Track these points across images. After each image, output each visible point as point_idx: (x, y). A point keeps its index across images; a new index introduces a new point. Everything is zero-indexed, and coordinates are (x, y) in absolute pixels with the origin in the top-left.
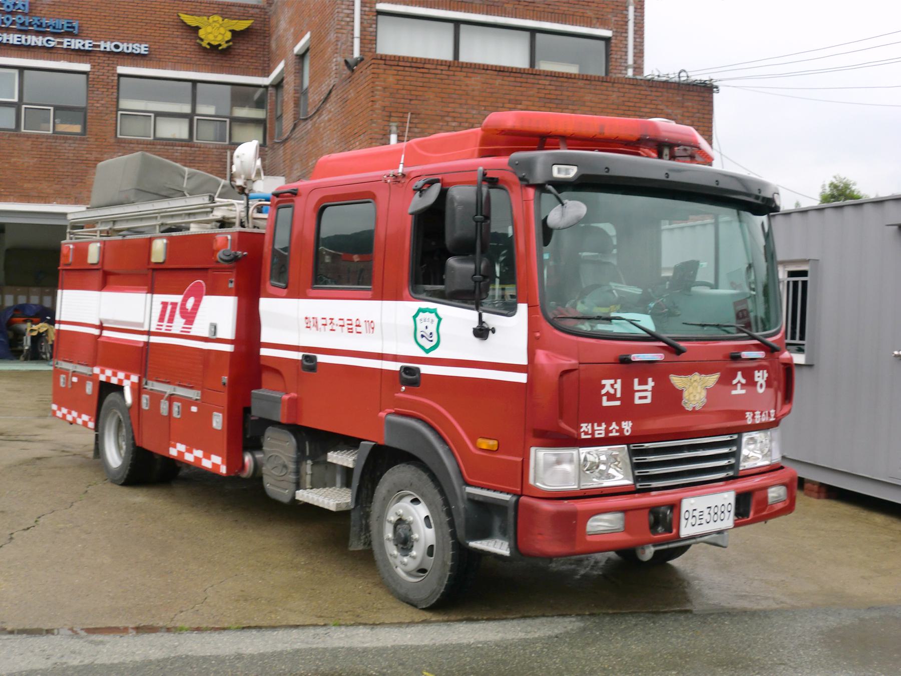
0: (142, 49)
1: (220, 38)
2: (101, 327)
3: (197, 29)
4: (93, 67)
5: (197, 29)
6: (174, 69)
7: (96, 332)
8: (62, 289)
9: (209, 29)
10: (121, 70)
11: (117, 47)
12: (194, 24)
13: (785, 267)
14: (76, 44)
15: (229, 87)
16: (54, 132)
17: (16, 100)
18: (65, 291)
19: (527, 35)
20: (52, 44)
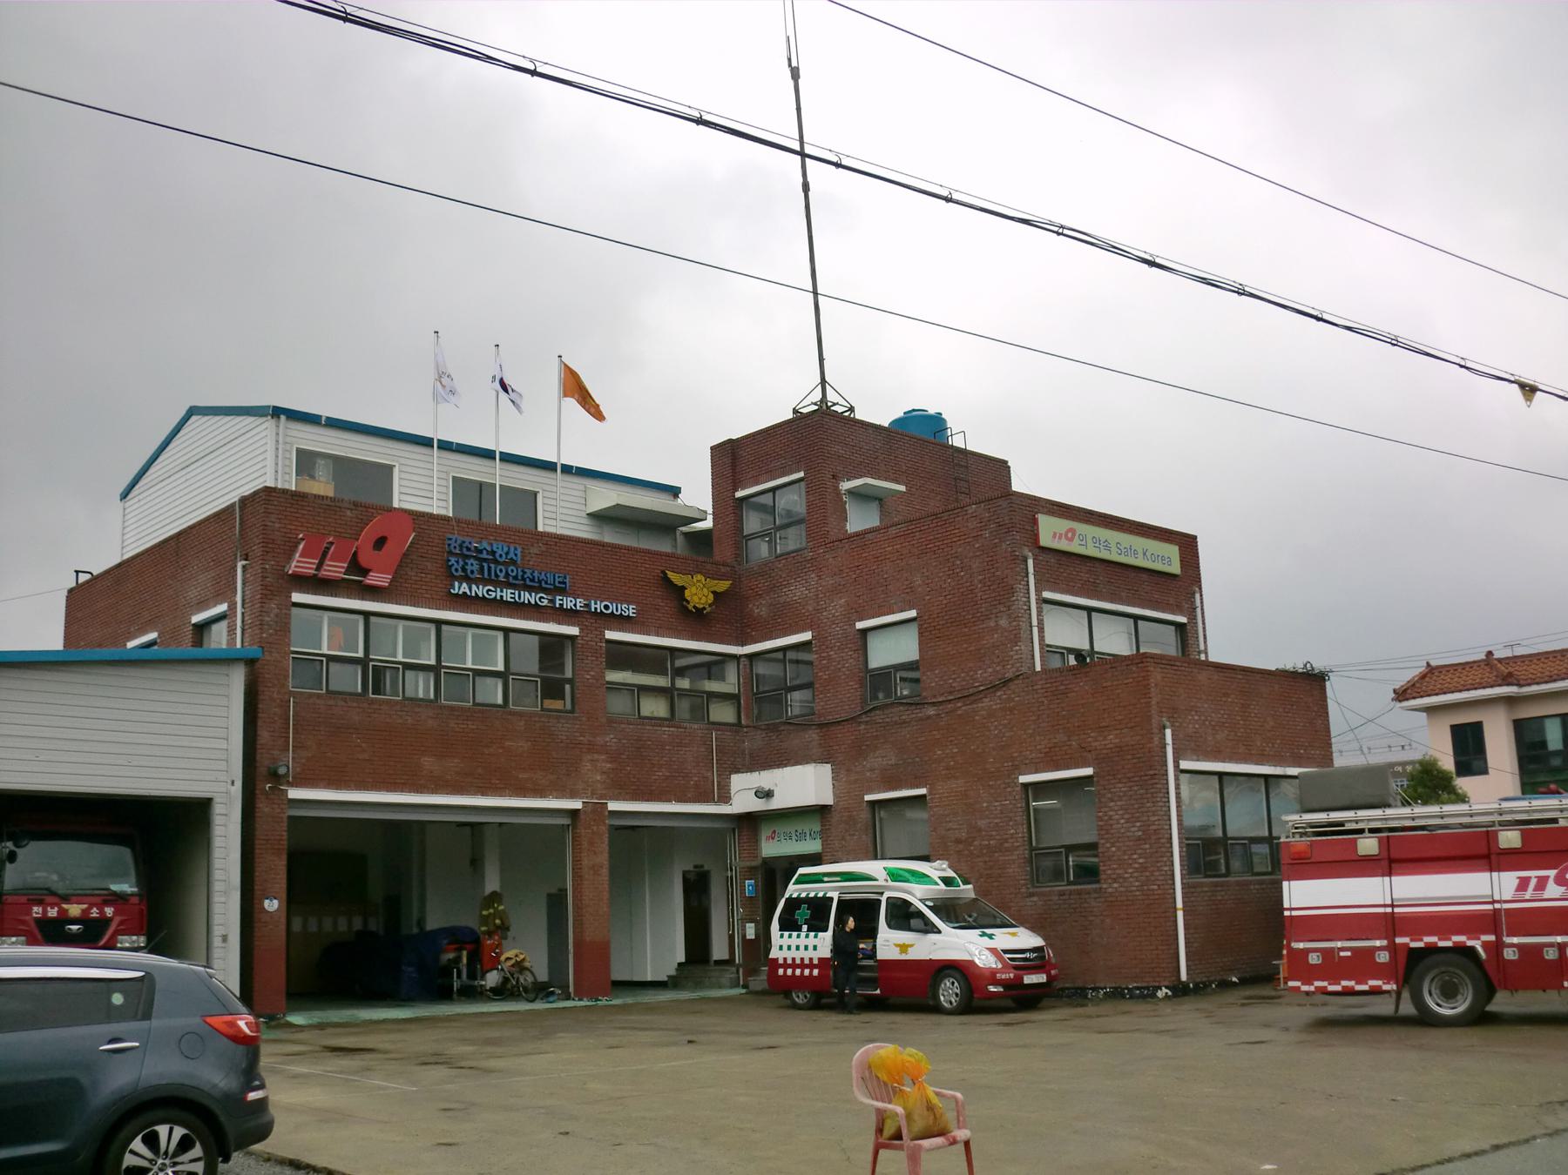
0: (631, 611)
1: (696, 599)
2: (1392, 906)
3: (683, 588)
4: (581, 630)
5: (683, 588)
6: (658, 635)
7: (1389, 910)
8: (1289, 880)
9: (694, 590)
10: (297, 597)
11: (606, 607)
12: (680, 584)
13: (205, 982)
14: (568, 603)
15: (536, 638)
16: (475, 704)
17: (360, 654)
18: (1293, 883)
19: (1085, 614)
20: (545, 602)
